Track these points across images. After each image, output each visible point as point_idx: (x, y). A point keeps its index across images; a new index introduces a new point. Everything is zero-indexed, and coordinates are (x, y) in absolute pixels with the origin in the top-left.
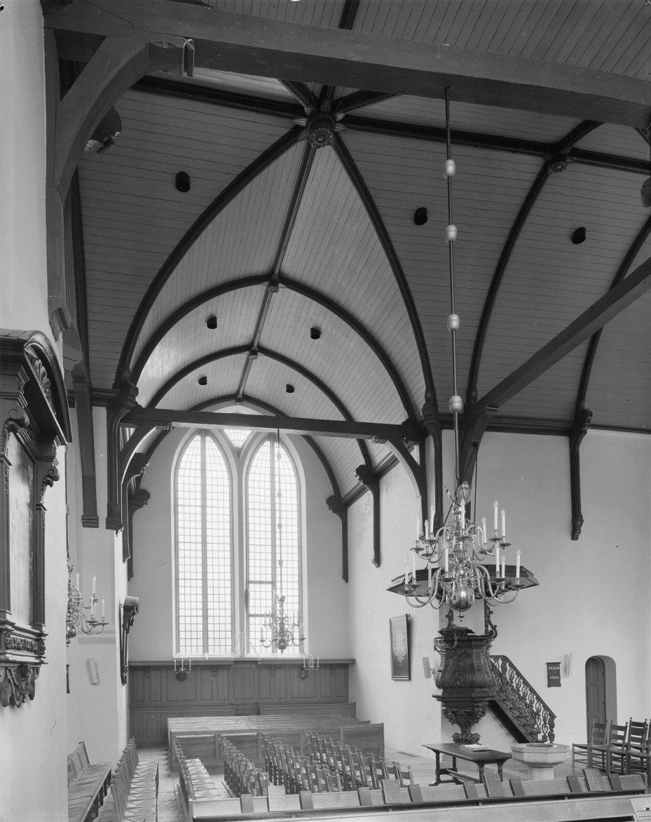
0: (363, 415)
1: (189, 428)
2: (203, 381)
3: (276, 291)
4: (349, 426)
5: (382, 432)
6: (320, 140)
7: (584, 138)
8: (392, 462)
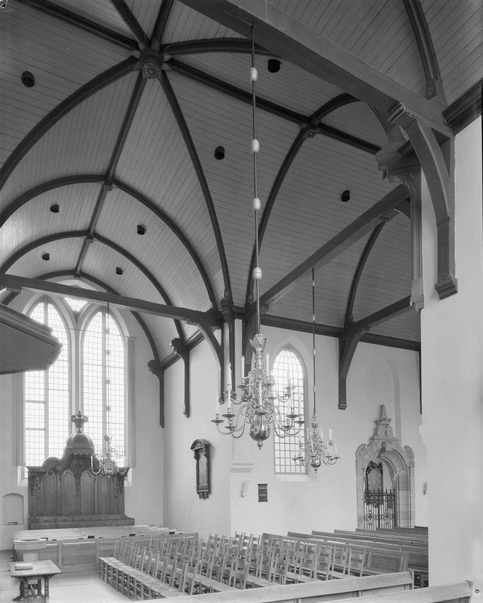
0: (180, 302)
1: (35, 293)
2: (46, 257)
3: (111, 190)
4: (169, 309)
5: (193, 316)
6: (150, 72)
7: (327, 116)
8: (199, 339)
